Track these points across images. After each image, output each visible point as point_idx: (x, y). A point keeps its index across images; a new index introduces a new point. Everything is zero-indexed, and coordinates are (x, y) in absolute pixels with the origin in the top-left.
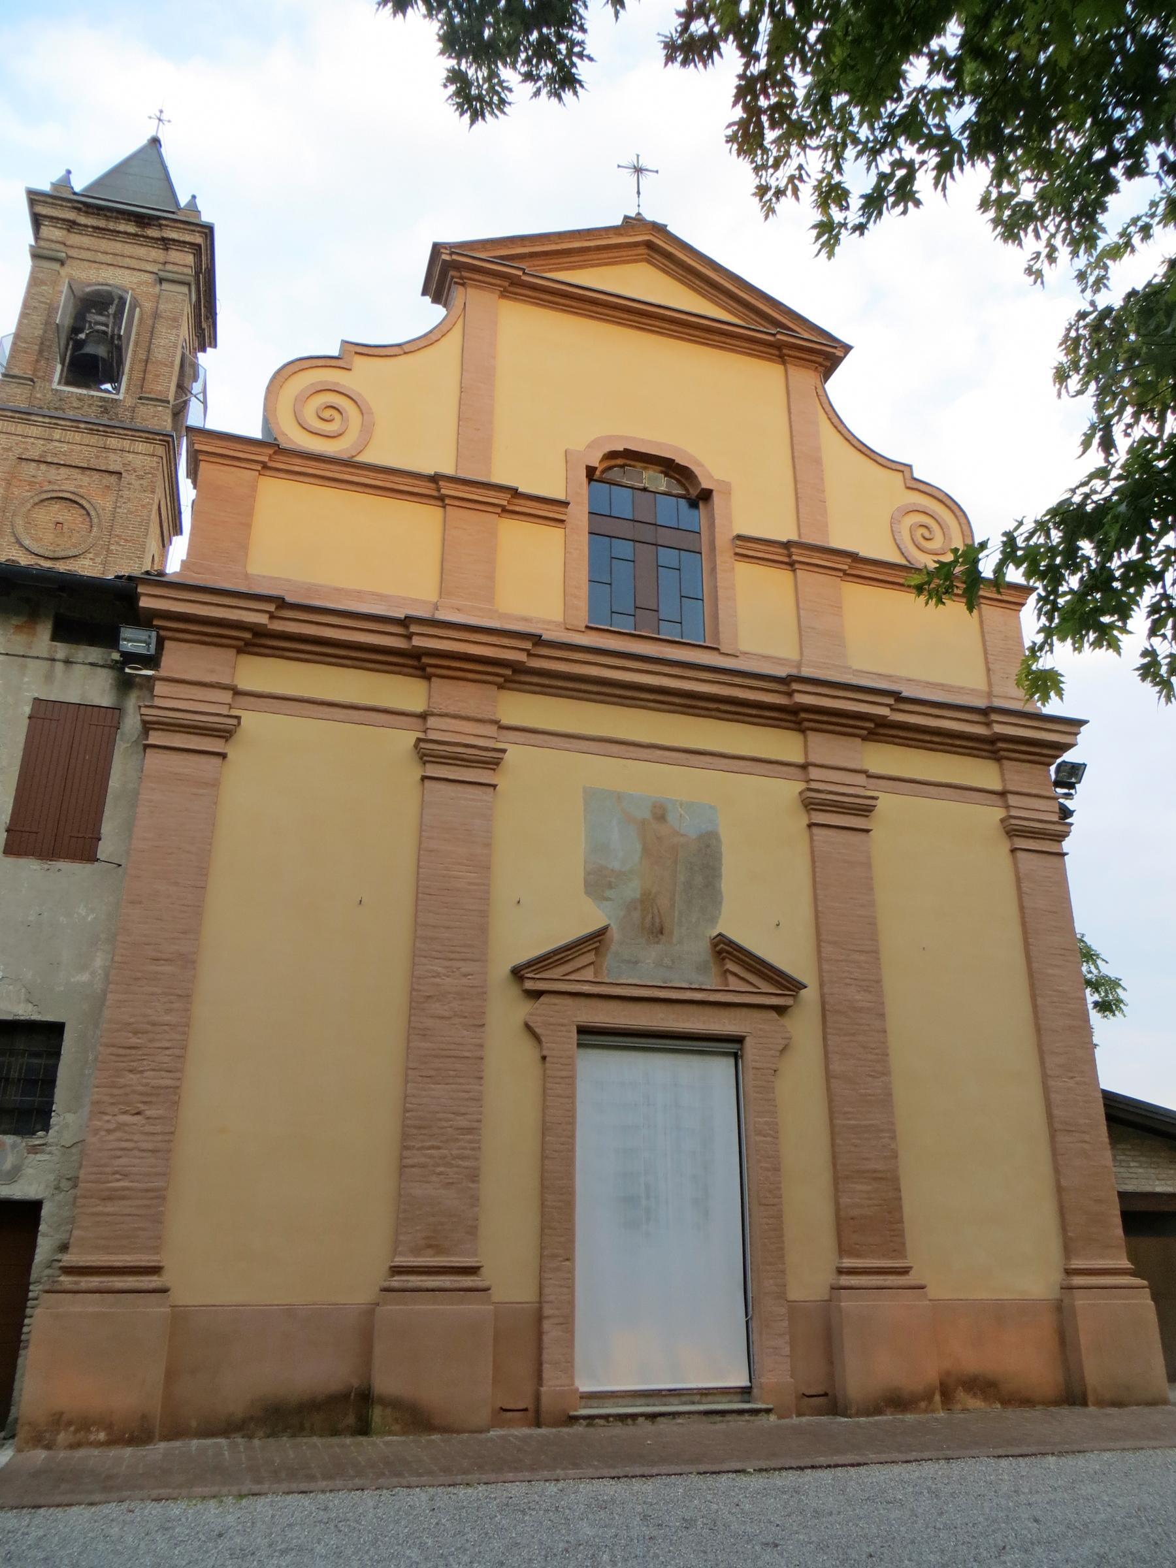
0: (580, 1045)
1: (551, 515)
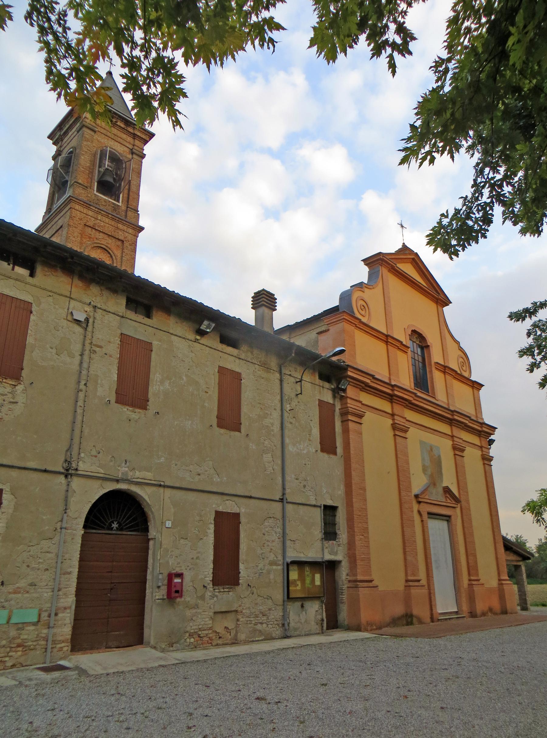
0: (429, 518)
1: (394, 343)
